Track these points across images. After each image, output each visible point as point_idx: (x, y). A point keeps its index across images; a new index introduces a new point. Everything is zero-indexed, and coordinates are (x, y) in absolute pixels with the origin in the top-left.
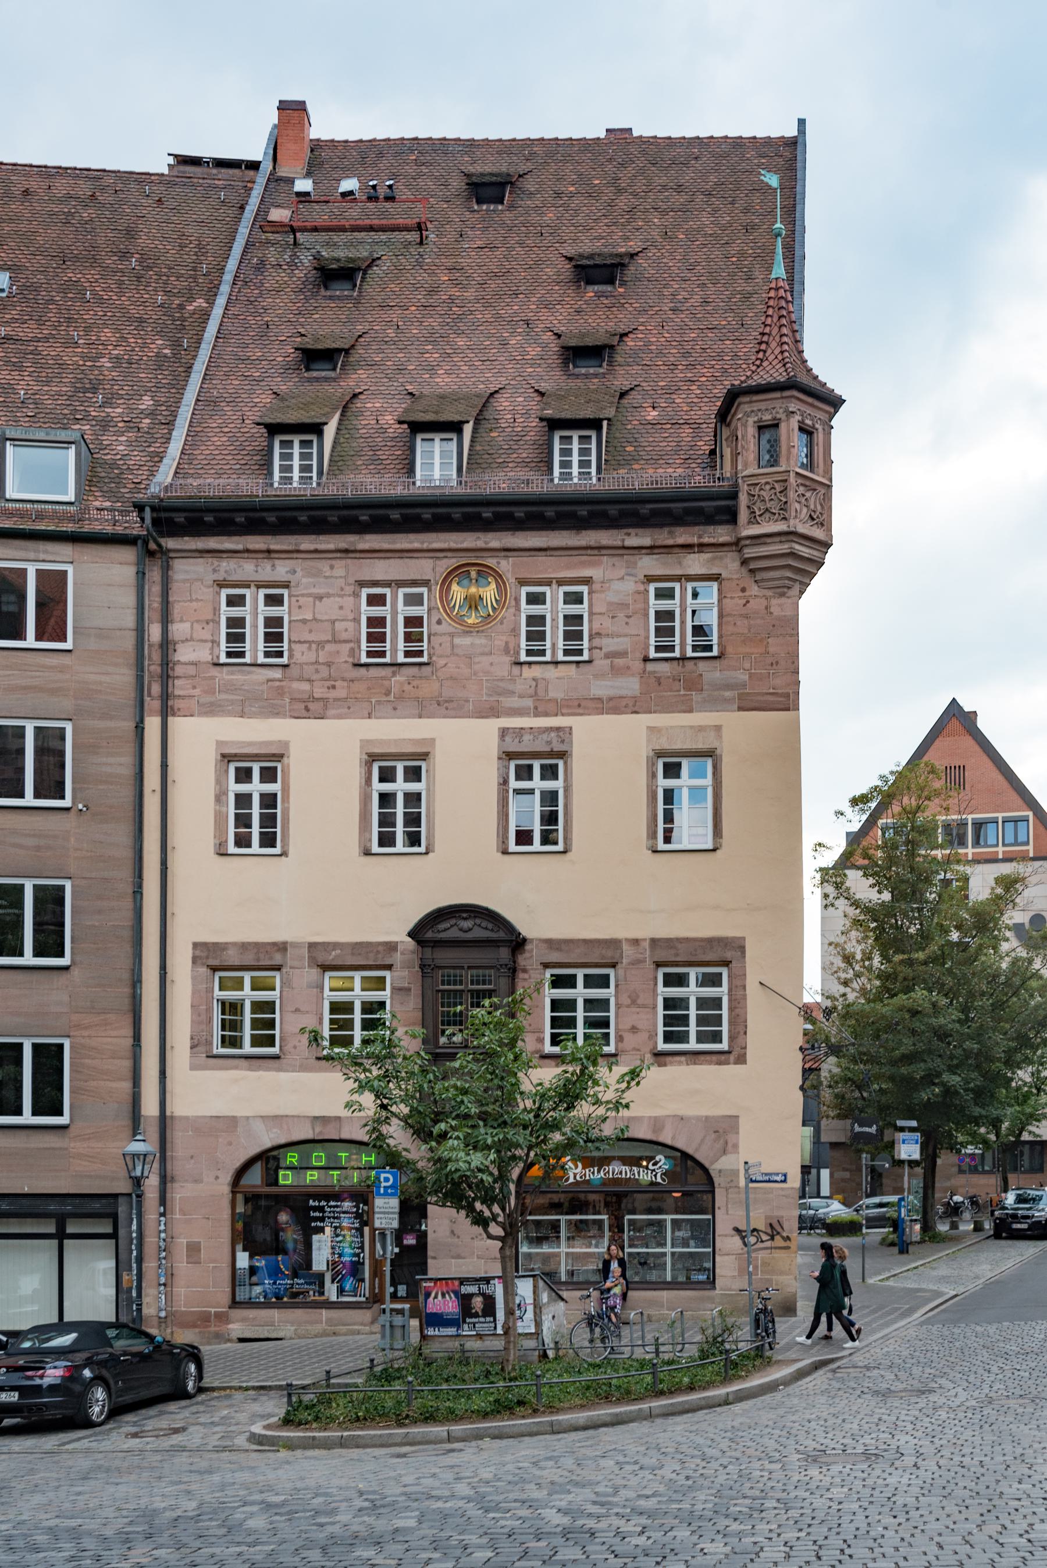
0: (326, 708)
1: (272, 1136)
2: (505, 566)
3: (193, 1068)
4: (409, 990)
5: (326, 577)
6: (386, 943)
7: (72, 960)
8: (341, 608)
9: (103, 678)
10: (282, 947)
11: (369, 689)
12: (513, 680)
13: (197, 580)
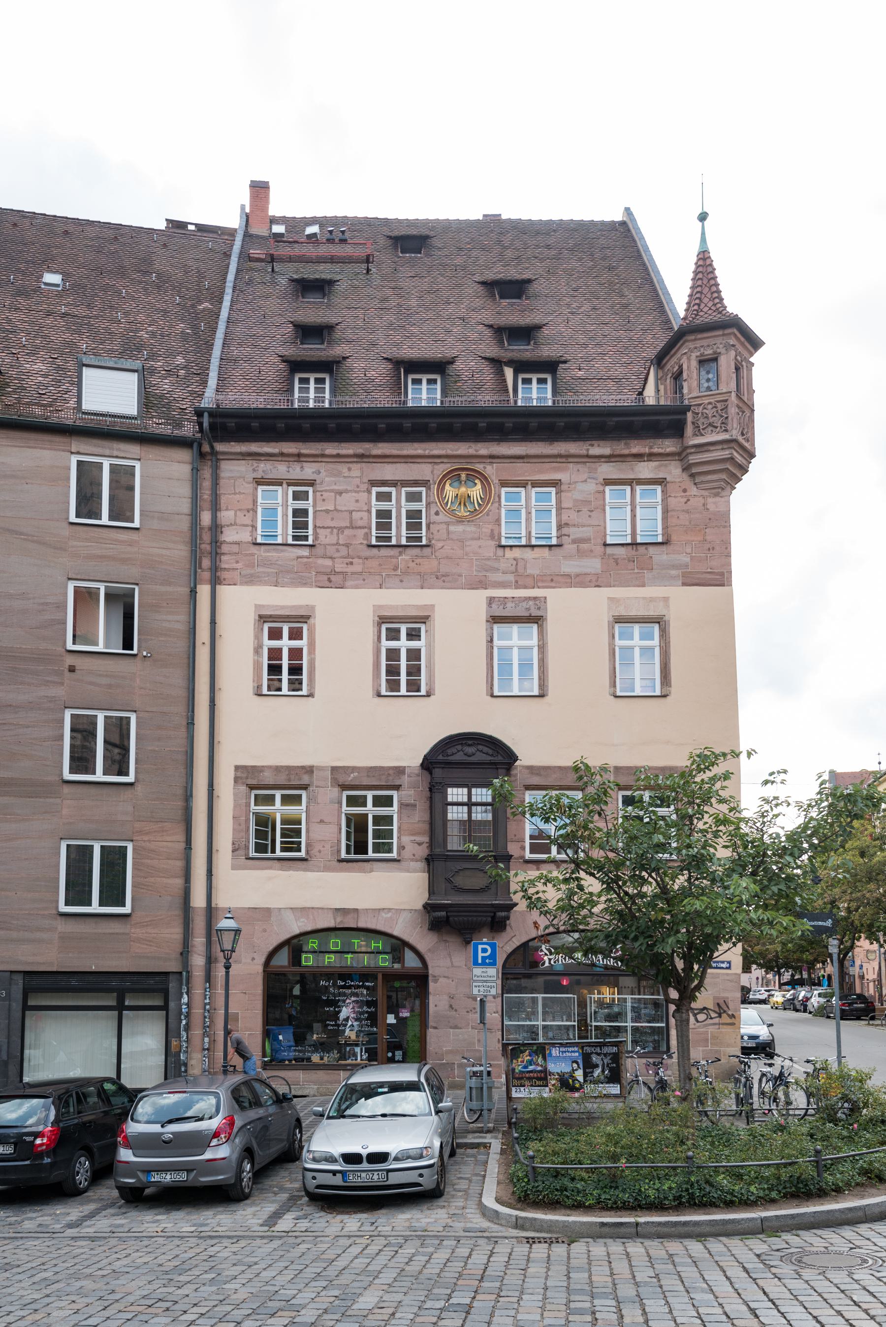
0: (345, 580)
1: (300, 924)
2: (490, 470)
3: (234, 868)
4: (415, 806)
5: (345, 477)
6: (396, 768)
7: (136, 778)
8: (357, 501)
9: (164, 552)
10: (309, 770)
11: (380, 565)
12: (497, 559)
13: (240, 477)
